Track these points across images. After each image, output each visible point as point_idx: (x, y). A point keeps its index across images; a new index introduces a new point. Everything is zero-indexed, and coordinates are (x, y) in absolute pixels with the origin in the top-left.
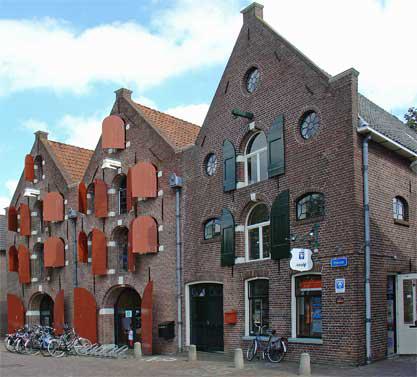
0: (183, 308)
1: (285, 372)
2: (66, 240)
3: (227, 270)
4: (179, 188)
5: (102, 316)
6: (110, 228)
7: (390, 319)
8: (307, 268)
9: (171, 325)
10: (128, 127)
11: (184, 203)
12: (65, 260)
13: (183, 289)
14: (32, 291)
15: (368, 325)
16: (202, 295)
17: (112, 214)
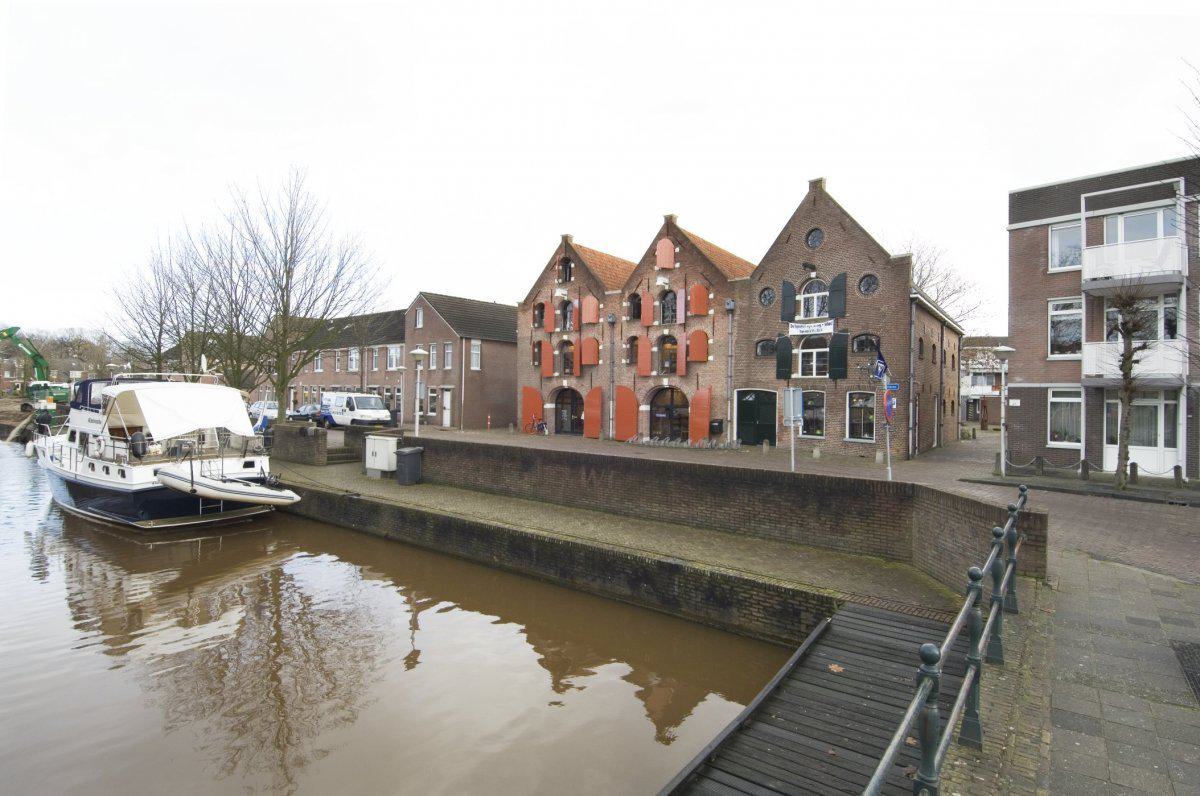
0: (732, 409)
1: (615, 555)
2: (601, 341)
3: (783, 382)
4: (731, 311)
5: (642, 412)
6: (654, 335)
7: (1035, 378)
8: (370, 437)
9: (721, 422)
10: (677, 250)
11: (736, 324)
12: (599, 358)
13: (732, 394)
14: (555, 384)
15: (911, 432)
16: (751, 399)
17: (558, 330)
